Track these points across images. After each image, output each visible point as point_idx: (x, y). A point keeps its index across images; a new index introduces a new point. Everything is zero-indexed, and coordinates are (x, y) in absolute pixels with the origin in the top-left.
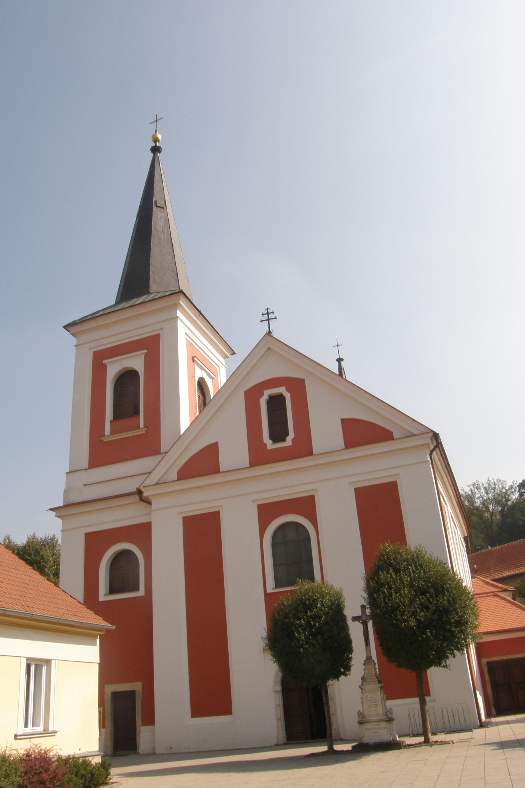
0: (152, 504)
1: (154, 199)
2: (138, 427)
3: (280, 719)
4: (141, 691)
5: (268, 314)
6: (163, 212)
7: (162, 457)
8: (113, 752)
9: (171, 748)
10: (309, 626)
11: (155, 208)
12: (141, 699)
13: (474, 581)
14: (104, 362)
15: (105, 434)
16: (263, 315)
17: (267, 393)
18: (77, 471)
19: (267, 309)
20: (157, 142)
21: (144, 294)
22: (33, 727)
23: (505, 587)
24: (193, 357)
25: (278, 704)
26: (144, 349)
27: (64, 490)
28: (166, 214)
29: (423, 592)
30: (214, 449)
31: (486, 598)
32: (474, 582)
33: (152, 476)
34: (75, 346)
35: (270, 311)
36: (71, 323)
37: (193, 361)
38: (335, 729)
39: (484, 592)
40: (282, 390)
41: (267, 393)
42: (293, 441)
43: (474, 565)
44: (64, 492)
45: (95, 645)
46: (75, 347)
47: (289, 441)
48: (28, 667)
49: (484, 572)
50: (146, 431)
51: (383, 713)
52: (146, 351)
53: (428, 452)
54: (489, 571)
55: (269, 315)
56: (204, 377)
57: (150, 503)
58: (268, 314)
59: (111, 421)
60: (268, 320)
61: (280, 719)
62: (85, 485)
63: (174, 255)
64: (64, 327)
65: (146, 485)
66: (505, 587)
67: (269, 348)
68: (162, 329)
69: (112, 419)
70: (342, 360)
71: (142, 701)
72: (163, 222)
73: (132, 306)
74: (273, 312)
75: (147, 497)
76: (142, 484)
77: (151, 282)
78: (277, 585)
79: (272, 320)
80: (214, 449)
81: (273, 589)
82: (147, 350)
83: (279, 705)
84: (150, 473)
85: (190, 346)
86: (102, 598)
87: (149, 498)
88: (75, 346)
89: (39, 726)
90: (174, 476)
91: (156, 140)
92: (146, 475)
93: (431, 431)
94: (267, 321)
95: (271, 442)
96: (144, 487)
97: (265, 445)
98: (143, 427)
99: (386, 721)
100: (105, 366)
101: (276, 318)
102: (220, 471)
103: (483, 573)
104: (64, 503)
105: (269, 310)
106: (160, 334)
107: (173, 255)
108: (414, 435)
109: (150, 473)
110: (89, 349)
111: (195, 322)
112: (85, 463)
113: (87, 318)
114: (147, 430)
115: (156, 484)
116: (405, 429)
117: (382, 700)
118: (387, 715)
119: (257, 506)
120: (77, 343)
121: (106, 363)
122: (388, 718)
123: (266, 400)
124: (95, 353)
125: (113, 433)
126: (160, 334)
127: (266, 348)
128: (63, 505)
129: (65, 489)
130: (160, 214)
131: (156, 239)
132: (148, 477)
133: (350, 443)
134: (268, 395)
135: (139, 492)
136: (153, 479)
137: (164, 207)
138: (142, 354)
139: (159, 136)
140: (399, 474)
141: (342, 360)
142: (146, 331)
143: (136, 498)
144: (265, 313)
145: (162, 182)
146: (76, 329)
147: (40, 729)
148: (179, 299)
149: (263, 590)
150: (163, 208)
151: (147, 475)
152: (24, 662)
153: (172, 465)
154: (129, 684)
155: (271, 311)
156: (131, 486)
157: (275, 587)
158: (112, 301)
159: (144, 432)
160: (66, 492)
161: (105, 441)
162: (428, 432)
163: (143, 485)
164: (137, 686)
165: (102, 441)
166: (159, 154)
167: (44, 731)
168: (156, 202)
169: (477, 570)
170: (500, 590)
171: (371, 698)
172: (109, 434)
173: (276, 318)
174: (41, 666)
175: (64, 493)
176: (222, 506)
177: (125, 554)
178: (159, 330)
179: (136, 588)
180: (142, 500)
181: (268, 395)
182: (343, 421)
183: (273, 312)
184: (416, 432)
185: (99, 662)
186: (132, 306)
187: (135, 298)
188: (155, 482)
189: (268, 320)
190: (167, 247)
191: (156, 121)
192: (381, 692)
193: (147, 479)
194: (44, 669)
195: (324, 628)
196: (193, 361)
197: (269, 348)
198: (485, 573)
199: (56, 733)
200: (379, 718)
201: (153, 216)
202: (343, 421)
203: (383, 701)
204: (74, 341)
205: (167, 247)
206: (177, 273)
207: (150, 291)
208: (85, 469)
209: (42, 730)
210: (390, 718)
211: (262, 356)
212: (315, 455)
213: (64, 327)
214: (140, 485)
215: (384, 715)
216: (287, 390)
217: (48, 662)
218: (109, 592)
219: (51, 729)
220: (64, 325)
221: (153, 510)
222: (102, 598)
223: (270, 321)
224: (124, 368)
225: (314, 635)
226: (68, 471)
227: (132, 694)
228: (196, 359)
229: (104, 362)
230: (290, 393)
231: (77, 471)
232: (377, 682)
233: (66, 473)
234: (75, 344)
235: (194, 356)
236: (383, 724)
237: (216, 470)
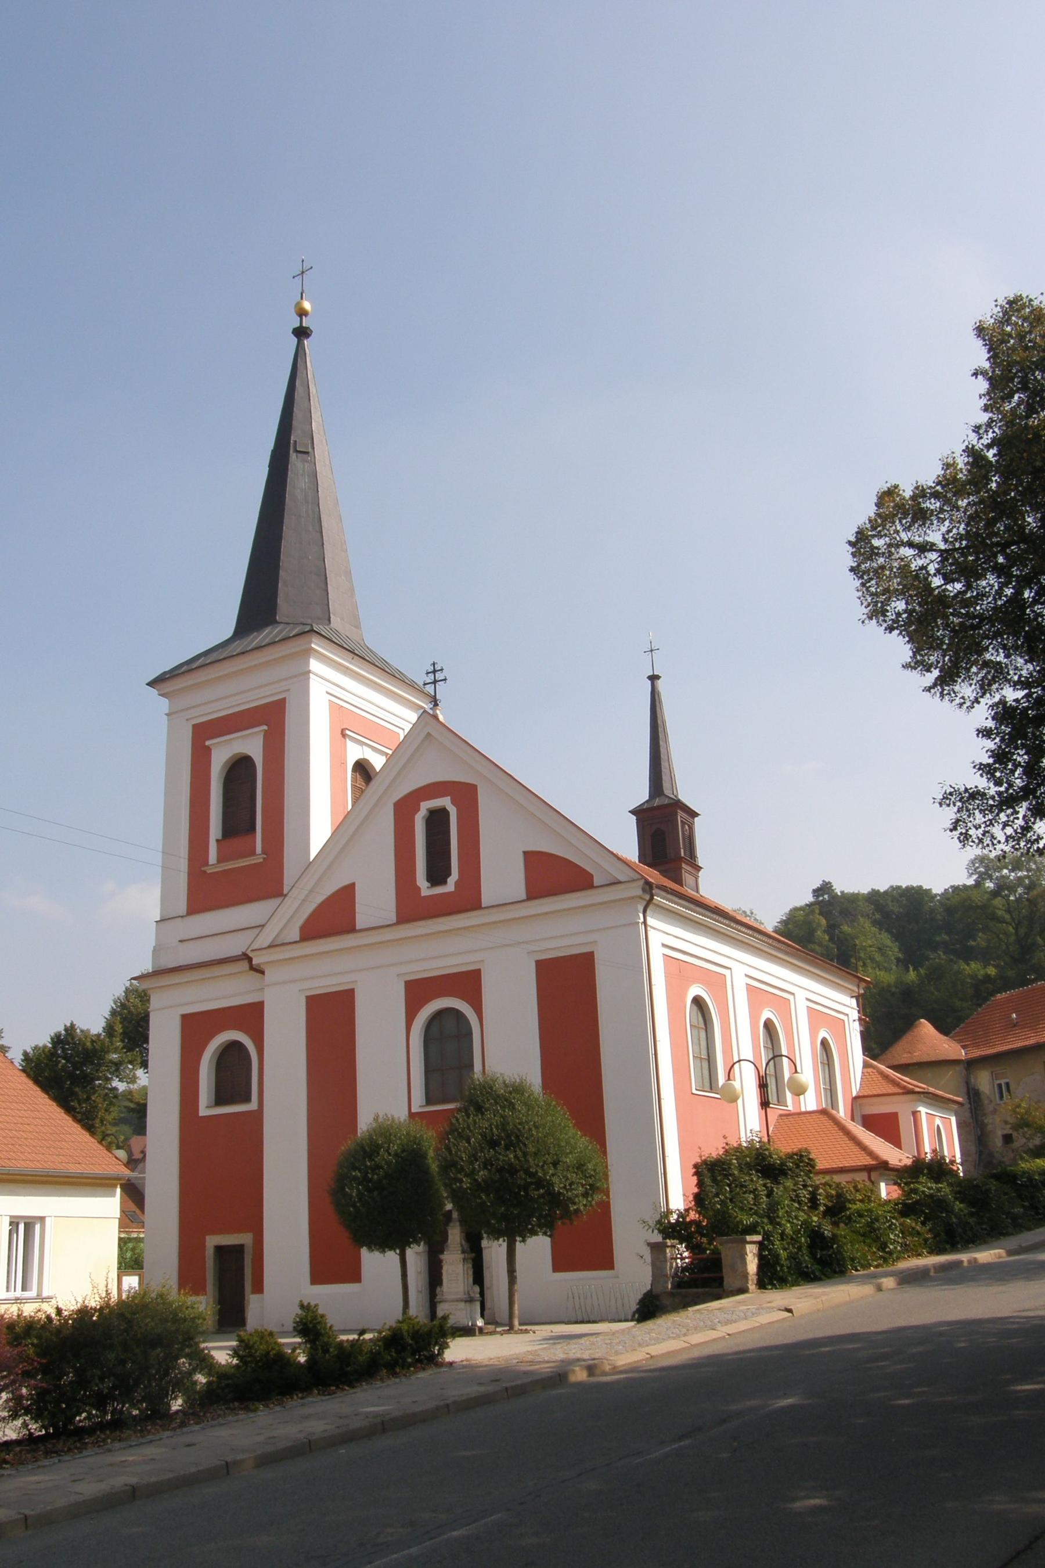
0: (266, 973)
1: (292, 437)
2: (253, 853)
3: (421, 1292)
4: (251, 1245)
5: (434, 672)
6: (307, 461)
7: (278, 905)
8: (217, 1327)
9: (283, 1325)
10: (365, 1179)
11: (293, 456)
12: (251, 1257)
13: (867, 1072)
14: (207, 743)
15: (208, 862)
16: (428, 673)
17: (426, 806)
18: (169, 919)
19: (434, 664)
20: (304, 317)
21: (267, 625)
22: (22, 1291)
23: (920, 1086)
24: (343, 730)
25: (419, 1270)
26: (261, 725)
27: (152, 949)
28: (313, 464)
29: (493, 1144)
30: (346, 895)
31: (797, 1116)
32: (866, 1074)
33: (267, 930)
34: (166, 714)
35: (438, 667)
36: (157, 677)
37: (344, 735)
38: (489, 1309)
39: (875, 1093)
40: (445, 802)
41: (426, 806)
42: (457, 884)
43: (1012, 1013)
44: (153, 951)
45: (114, 1195)
46: (166, 717)
47: (450, 886)
48: (14, 1223)
49: (1028, 1027)
50: (264, 859)
51: (464, 1291)
52: (265, 727)
53: (641, 908)
54: (1035, 1026)
55: (436, 674)
56: (365, 757)
57: (263, 973)
58: (434, 672)
59: (217, 841)
60: (435, 682)
61: (421, 1292)
62: (180, 941)
63: (323, 544)
64: (147, 684)
65: (254, 948)
66: (920, 1086)
67: (429, 734)
68: (289, 690)
69: (220, 837)
70: (658, 677)
71: (252, 1259)
72: (307, 480)
73: (243, 653)
74: (442, 670)
75: (259, 965)
76: (250, 945)
77: (280, 601)
78: (429, 1101)
79: (440, 683)
80: (346, 895)
81: (420, 1106)
82: (266, 725)
83: (420, 1273)
84: (263, 926)
85: (337, 710)
86: (203, 1112)
87: (262, 966)
88: (166, 714)
89: (31, 1290)
90: (295, 934)
91: (302, 313)
92: (260, 929)
93: (639, 877)
94: (433, 685)
95: (427, 884)
96: (252, 950)
97: (419, 889)
98: (260, 853)
99: (466, 1301)
100: (208, 750)
101: (445, 680)
102: (357, 928)
103: (1026, 1030)
104: (153, 968)
105: (436, 666)
106: (285, 699)
107: (321, 544)
108: (620, 882)
109: (263, 926)
110: (187, 720)
111: (347, 668)
112: (182, 907)
113: (180, 671)
114: (265, 856)
115: (270, 946)
116: (611, 874)
117: (464, 1274)
118: (469, 1294)
119: (403, 985)
120: (169, 709)
121: (211, 745)
122: (470, 1297)
123: (423, 818)
124: (195, 726)
125: (221, 859)
126: (285, 699)
127: (423, 735)
128: (153, 972)
129: (154, 947)
130: (302, 467)
131: (293, 517)
132: (260, 932)
133: (533, 894)
134: (427, 810)
135: (246, 957)
136: (266, 938)
137: (310, 450)
138: (261, 731)
139: (307, 305)
140: (596, 942)
141: (658, 677)
142: (262, 695)
143: (245, 965)
144: (430, 671)
145: (310, 400)
146: (169, 686)
147: (33, 1293)
148: (311, 642)
149: (407, 1109)
150: (307, 453)
151: (257, 931)
152: (7, 1220)
153: (292, 917)
154: (236, 1235)
155: (439, 668)
156: (234, 946)
157: (424, 1104)
158: (228, 629)
159: (261, 860)
160: (156, 951)
161: (209, 872)
162: (638, 879)
163: (250, 949)
164: (245, 1239)
165: (205, 872)
166: (305, 342)
167: (38, 1296)
168: (295, 442)
169: (1017, 1023)
170: (901, 1091)
171: (453, 1271)
172: (215, 862)
173: (445, 680)
174: (34, 1224)
175: (153, 954)
176: (356, 981)
177: (235, 1046)
178: (284, 691)
179: (247, 1099)
180: (253, 968)
181: (427, 810)
182: (525, 853)
183: (442, 670)
184: (622, 879)
185: (119, 1216)
186: (243, 653)
187: (253, 633)
188: (268, 944)
189: (435, 682)
190: (311, 529)
191: (303, 272)
192: (464, 1265)
193: (257, 939)
194: (38, 1227)
195: (384, 1182)
196: (344, 735)
197: (429, 734)
198: (1029, 1029)
199: (52, 1298)
200: (459, 1296)
201: (289, 473)
202: (525, 853)
203: (466, 1276)
204: (164, 704)
205: (311, 529)
206: (326, 578)
207: (277, 618)
208: (182, 917)
209: (35, 1295)
210: (473, 1297)
211: (423, 742)
212: (485, 908)
213: (147, 684)
214: (247, 950)
215: (465, 1294)
216: (453, 802)
217: (42, 1219)
218: (214, 1103)
219: (45, 1294)
220: (148, 681)
221: (268, 986)
222: (203, 1112)
223: (437, 685)
224: (235, 755)
225: (370, 1191)
226: (158, 919)
227: (239, 1249)
228: (348, 732)
229: (207, 743)
230: (456, 807)
231: (169, 919)
232: (460, 1252)
233: (156, 922)
234: (167, 712)
235: (344, 727)
236: (462, 1305)
237: (349, 927)
